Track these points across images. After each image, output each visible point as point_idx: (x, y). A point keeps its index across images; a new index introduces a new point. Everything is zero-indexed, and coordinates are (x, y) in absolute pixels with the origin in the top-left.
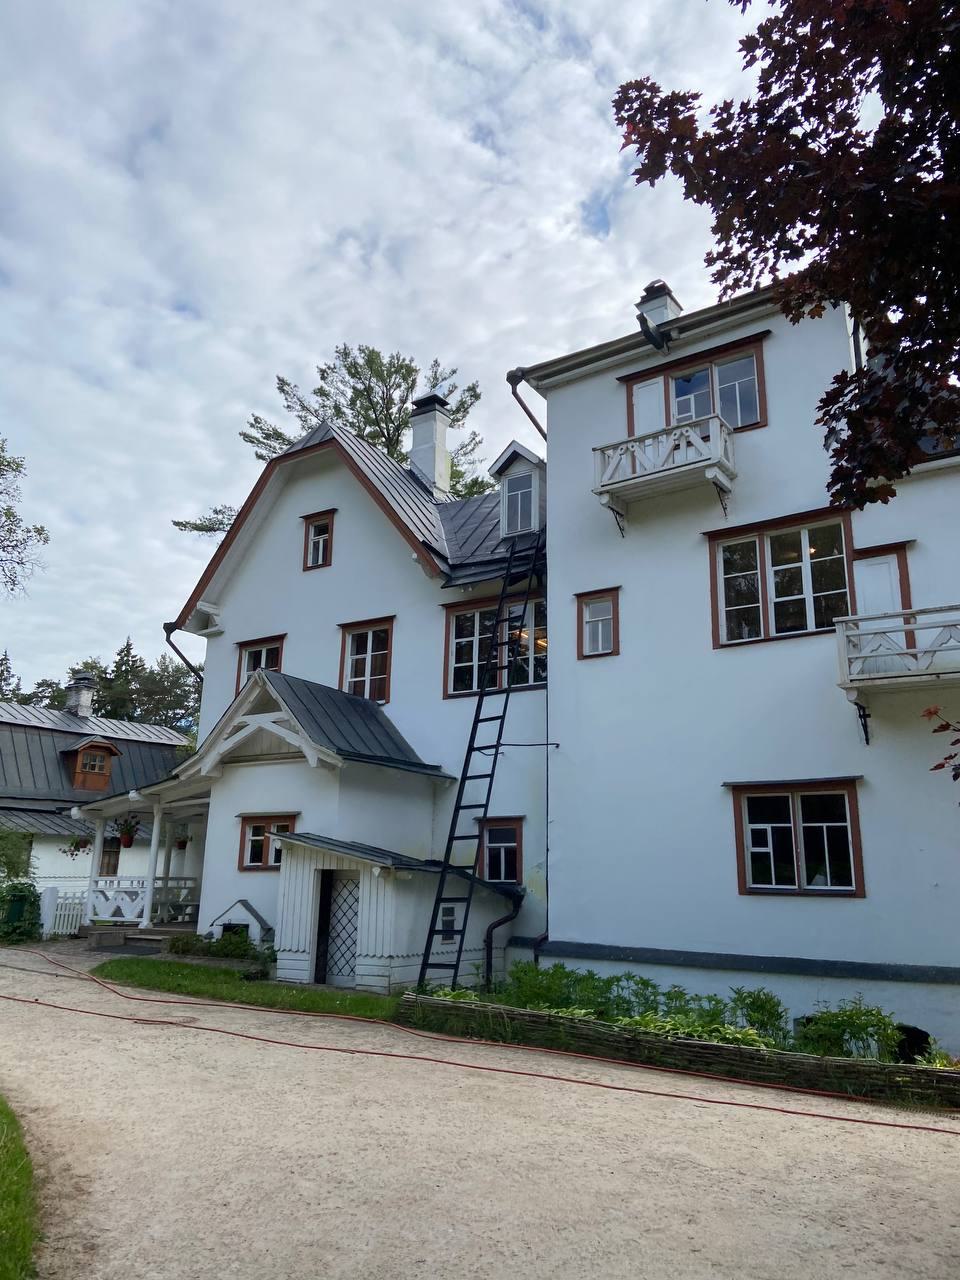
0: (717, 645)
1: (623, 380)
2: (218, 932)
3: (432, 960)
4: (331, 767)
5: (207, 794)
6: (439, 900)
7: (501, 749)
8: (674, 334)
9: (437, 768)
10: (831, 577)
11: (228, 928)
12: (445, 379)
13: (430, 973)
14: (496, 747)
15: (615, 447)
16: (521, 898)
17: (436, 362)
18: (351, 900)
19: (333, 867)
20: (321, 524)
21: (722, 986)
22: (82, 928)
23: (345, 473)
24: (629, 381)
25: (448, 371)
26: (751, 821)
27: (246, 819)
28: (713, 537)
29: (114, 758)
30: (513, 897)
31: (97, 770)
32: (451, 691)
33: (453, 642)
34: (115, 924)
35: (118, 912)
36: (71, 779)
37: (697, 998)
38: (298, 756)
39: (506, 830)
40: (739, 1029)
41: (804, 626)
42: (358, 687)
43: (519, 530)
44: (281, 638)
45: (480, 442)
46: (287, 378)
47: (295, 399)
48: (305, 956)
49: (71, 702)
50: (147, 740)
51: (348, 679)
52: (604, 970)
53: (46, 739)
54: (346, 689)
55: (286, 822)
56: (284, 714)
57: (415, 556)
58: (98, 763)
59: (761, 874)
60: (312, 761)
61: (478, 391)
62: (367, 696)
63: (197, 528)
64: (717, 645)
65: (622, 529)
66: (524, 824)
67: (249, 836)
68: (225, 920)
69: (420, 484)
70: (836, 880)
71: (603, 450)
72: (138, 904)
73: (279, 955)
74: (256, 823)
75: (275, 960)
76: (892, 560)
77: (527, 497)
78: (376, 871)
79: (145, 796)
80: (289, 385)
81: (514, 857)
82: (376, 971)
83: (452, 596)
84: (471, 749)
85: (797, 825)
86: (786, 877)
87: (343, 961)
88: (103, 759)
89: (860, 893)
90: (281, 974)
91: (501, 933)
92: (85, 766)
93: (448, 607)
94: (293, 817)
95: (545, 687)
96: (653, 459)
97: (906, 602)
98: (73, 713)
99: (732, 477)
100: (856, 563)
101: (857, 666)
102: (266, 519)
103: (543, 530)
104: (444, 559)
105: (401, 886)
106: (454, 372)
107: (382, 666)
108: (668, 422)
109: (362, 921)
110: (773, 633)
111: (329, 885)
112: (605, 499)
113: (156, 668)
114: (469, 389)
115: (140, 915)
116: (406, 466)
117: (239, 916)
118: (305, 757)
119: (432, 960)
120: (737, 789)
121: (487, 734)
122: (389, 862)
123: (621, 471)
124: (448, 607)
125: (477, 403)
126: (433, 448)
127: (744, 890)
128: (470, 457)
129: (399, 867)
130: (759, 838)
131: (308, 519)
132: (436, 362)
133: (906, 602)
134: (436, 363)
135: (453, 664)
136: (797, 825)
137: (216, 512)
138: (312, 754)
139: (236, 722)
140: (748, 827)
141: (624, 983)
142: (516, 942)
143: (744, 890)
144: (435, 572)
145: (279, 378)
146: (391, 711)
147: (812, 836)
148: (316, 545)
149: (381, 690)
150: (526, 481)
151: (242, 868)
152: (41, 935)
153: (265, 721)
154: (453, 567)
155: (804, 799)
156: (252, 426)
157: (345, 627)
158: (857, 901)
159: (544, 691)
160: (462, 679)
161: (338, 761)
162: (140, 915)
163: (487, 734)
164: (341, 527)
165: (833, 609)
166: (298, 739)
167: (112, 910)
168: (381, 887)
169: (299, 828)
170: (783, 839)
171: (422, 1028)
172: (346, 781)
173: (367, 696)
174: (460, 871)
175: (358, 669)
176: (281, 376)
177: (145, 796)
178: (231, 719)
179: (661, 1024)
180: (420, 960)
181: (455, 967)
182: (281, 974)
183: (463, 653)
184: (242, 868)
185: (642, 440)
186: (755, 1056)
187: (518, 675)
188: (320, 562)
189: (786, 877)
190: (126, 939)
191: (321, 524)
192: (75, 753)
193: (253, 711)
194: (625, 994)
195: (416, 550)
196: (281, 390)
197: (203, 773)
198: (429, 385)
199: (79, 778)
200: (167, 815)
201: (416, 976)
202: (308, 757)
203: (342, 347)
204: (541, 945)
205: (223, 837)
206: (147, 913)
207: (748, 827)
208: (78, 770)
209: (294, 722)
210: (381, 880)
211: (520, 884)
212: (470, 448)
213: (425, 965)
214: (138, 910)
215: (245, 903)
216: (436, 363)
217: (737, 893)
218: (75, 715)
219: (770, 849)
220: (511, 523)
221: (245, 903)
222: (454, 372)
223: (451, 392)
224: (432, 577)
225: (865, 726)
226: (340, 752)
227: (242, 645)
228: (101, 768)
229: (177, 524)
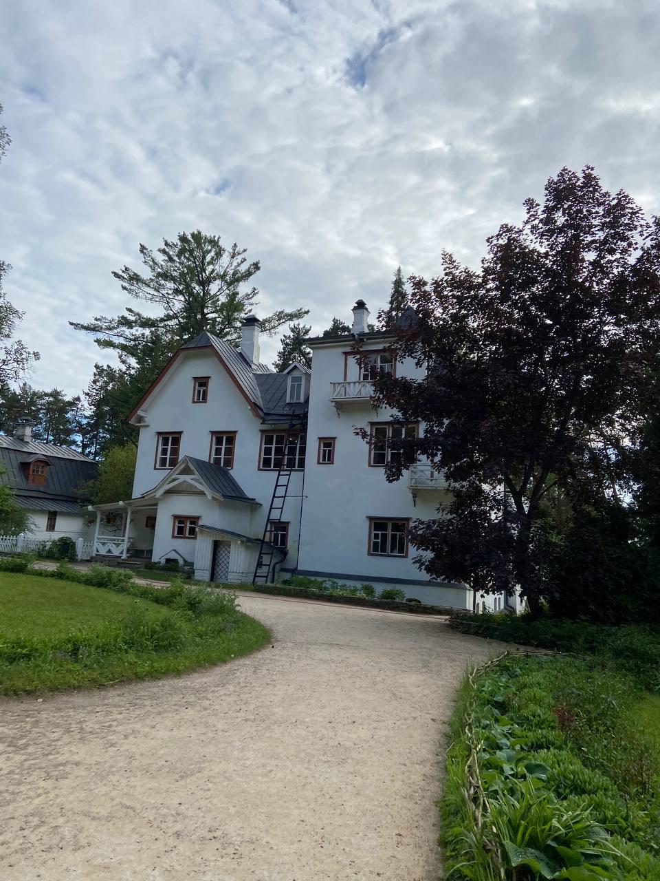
2: (163, 561)
3: (257, 574)
4: (216, 499)
5: (156, 505)
6: (261, 553)
8: (365, 340)
9: (254, 499)
11: (168, 561)
12: (239, 254)
14: (284, 497)
15: (339, 384)
16: (287, 553)
17: (235, 244)
18: (226, 552)
19: (220, 539)
21: (358, 585)
22: (92, 557)
23: (216, 360)
25: (242, 250)
27: (175, 517)
29: (48, 467)
30: (284, 553)
31: (40, 473)
33: (264, 446)
34: (108, 556)
35: (109, 551)
36: (27, 477)
37: (350, 587)
38: (202, 493)
40: (361, 594)
42: (217, 461)
43: (295, 401)
44: (180, 433)
45: (257, 293)
46: (146, 246)
47: (150, 258)
48: (207, 572)
50: (58, 456)
51: (213, 456)
52: (320, 579)
53: (12, 455)
54: (212, 462)
55: (194, 520)
56: (197, 476)
57: (249, 408)
59: (376, 549)
60: (210, 497)
61: (259, 265)
62: (222, 465)
63: (84, 327)
64: (370, 465)
65: (339, 415)
66: (289, 525)
67: (177, 524)
68: (168, 557)
69: (245, 361)
70: (399, 552)
71: (334, 384)
72: (120, 549)
74: (180, 519)
75: (194, 573)
77: (299, 386)
78: (239, 542)
79: (126, 504)
80: (146, 249)
81: (284, 538)
82: (236, 577)
83: (264, 427)
85: (390, 533)
86: (384, 550)
87: (222, 574)
88: (43, 467)
90: (196, 578)
91: (278, 566)
92: (34, 471)
93: (262, 431)
94: (198, 518)
95: (303, 471)
98: (21, 439)
101: (413, 481)
102: (173, 374)
103: (307, 401)
104: (262, 410)
105: (247, 548)
106: (245, 251)
107: (230, 452)
108: (360, 379)
109: (231, 560)
111: (216, 545)
112: (334, 404)
113: (18, 392)
114: (254, 264)
115: (122, 553)
116: (239, 350)
117: (173, 556)
118: (205, 494)
119: (257, 574)
120: (370, 519)
121: (281, 491)
122: (245, 540)
123: (340, 394)
124: (262, 431)
125: (257, 272)
126: (253, 344)
127: (369, 554)
128: (250, 301)
129: (248, 542)
130: (376, 536)
132: (235, 244)
134: (235, 245)
135: (263, 456)
136: (390, 533)
137: (96, 319)
138: (209, 494)
139: (173, 477)
140: (373, 532)
141: (328, 582)
142: (283, 570)
143: (369, 554)
144: (257, 415)
145: (141, 245)
146: (234, 473)
147: (394, 537)
148: (199, 391)
149: (229, 462)
150: (299, 379)
151: (174, 537)
152: (77, 560)
153: (188, 478)
154: (266, 414)
155: (393, 524)
156: (123, 272)
160: (267, 463)
161: (222, 499)
162: (122, 553)
164: (212, 386)
167: (107, 550)
168: (240, 549)
169: (201, 523)
170: (384, 536)
171: (265, 593)
172: (222, 505)
173: (222, 465)
175: (218, 452)
176: (142, 244)
177: (126, 504)
178: (171, 476)
179: (338, 592)
180: (253, 575)
182: (196, 578)
183: (268, 451)
184: (174, 537)
185: (349, 383)
186: (364, 600)
187: (291, 464)
189: (384, 550)
192: (29, 464)
194: (327, 586)
195: (250, 405)
196: (142, 251)
197: (157, 497)
198: (230, 257)
199: (31, 478)
201: (252, 579)
203: (182, 234)
204: (294, 571)
205: (164, 525)
206: (125, 552)
208: (31, 473)
209: (202, 480)
211: (286, 547)
212: (251, 296)
213: (255, 576)
214: (120, 551)
215: (175, 550)
216: (235, 245)
217: (366, 554)
218: (22, 440)
219: (379, 540)
220: (292, 396)
222: (245, 251)
223: (242, 262)
225: (415, 502)
227: (159, 434)
228: (42, 472)
229: (72, 324)
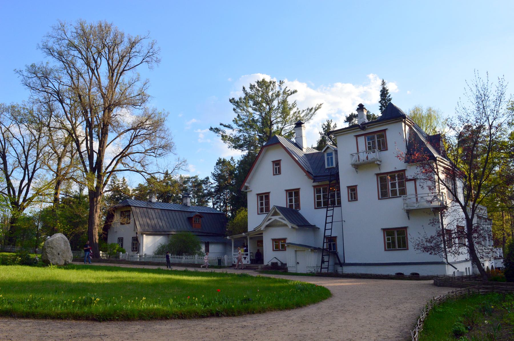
0: (379, 199)
1: (357, 136)
3: (322, 267)
5: (262, 234)
6: (323, 255)
7: (333, 223)
9: (315, 226)
10: (402, 185)
13: (322, 269)
14: (332, 223)
20: (277, 163)
24: (357, 136)
26: (387, 236)
28: (377, 175)
30: (335, 254)
32: (316, 207)
36: (192, 226)
38: (286, 225)
39: (331, 240)
41: (396, 195)
42: (291, 206)
49: (184, 202)
51: (288, 204)
54: (288, 207)
56: (282, 216)
57: (305, 174)
58: (197, 220)
60: (290, 227)
62: (294, 208)
64: (379, 199)
67: (274, 244)
73: (288, 268)
74: (275, 240)
76: (413, 182)
77: (332, 158)
78: (310, 250)
84: (326, 223)
86: (394, 246)
89: (408, 249)
90: (289, 271)
93: (314, 187)
96: (363, 157)
97: (416, 193)
99: (381, 162)
100: (406, 182)
102: (260, 162)
107: (297, 201)
110: (390, 196)
117: (275, 261)
120: (384, 230)
121: (329, 220)
124: (314, 187)
130: (388, 239)
131: (273, 162)
133: (416, 193)
138: (290, 225)
148: (276, 168)
149: (298, 206)
153: (276, 218)
154: (315, 177)
157: (287, 191)
158: (407, 251)
159: (340, 208)
161: (297, 227)
162: (248, 262)
163: (329, 220)
164: (283, 166)
165: (403, 192)
166: (286, 222)
170: (393, 239)
173: (294, 208)
174: (326, 249)
175: (291, 201)
180: (320, 267)
181: (328, 268)
182: (289, 271)
183: (319, 198)
188: (278, 173)
190: (246, 267)
191: (277, 163)
192: (192, 218)
193: (273, 215)
195: (305, 172)
200: (251, 238)
202: (288, 225)
207: (386, 237)
209: (284, 218)
210: (310, 252)
213: (321, 268)
215: (275, 258)
218: (187, 205)
221: (275, 258)
224: (309, 178)
226: (297, 225)
228: (199, 222)
